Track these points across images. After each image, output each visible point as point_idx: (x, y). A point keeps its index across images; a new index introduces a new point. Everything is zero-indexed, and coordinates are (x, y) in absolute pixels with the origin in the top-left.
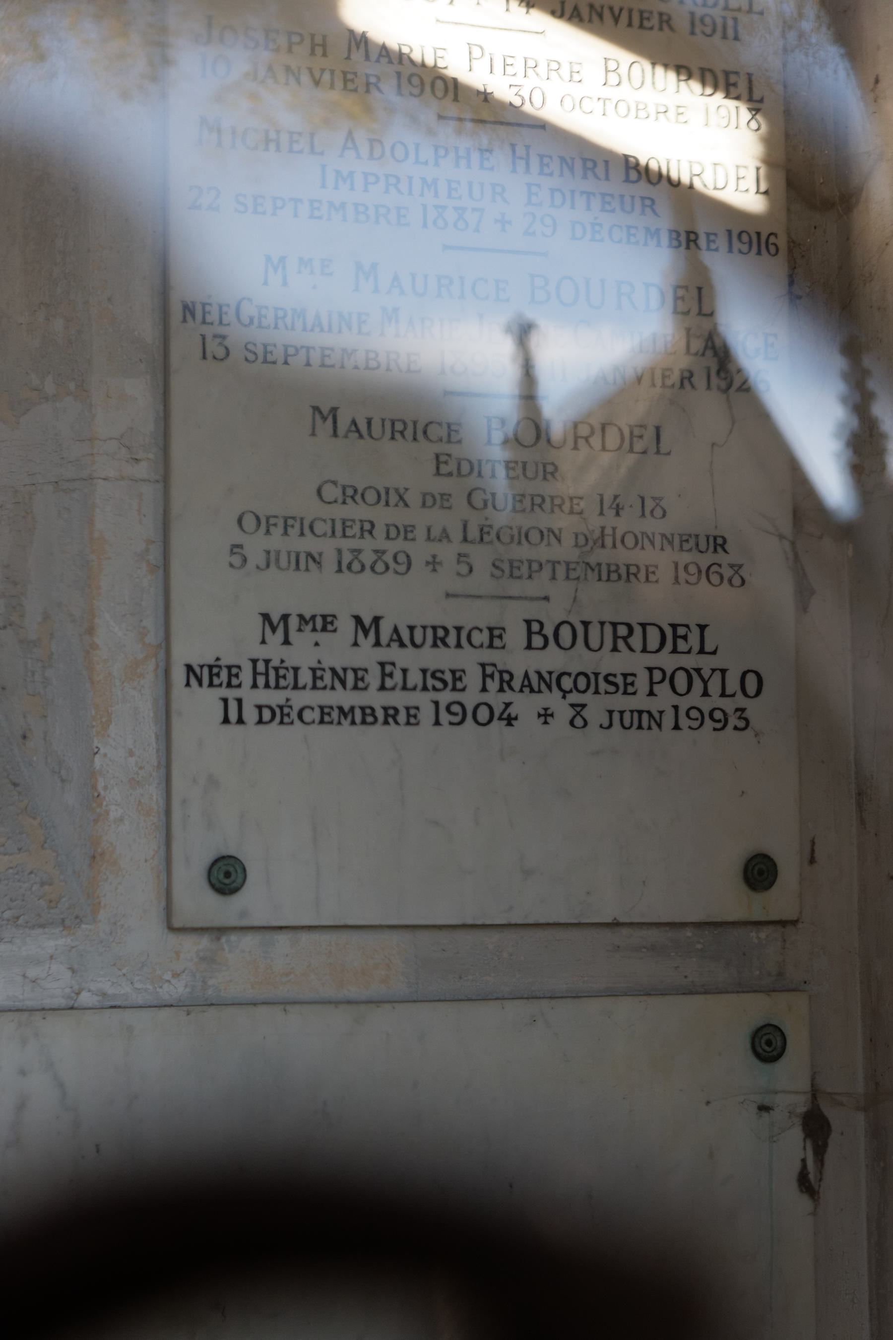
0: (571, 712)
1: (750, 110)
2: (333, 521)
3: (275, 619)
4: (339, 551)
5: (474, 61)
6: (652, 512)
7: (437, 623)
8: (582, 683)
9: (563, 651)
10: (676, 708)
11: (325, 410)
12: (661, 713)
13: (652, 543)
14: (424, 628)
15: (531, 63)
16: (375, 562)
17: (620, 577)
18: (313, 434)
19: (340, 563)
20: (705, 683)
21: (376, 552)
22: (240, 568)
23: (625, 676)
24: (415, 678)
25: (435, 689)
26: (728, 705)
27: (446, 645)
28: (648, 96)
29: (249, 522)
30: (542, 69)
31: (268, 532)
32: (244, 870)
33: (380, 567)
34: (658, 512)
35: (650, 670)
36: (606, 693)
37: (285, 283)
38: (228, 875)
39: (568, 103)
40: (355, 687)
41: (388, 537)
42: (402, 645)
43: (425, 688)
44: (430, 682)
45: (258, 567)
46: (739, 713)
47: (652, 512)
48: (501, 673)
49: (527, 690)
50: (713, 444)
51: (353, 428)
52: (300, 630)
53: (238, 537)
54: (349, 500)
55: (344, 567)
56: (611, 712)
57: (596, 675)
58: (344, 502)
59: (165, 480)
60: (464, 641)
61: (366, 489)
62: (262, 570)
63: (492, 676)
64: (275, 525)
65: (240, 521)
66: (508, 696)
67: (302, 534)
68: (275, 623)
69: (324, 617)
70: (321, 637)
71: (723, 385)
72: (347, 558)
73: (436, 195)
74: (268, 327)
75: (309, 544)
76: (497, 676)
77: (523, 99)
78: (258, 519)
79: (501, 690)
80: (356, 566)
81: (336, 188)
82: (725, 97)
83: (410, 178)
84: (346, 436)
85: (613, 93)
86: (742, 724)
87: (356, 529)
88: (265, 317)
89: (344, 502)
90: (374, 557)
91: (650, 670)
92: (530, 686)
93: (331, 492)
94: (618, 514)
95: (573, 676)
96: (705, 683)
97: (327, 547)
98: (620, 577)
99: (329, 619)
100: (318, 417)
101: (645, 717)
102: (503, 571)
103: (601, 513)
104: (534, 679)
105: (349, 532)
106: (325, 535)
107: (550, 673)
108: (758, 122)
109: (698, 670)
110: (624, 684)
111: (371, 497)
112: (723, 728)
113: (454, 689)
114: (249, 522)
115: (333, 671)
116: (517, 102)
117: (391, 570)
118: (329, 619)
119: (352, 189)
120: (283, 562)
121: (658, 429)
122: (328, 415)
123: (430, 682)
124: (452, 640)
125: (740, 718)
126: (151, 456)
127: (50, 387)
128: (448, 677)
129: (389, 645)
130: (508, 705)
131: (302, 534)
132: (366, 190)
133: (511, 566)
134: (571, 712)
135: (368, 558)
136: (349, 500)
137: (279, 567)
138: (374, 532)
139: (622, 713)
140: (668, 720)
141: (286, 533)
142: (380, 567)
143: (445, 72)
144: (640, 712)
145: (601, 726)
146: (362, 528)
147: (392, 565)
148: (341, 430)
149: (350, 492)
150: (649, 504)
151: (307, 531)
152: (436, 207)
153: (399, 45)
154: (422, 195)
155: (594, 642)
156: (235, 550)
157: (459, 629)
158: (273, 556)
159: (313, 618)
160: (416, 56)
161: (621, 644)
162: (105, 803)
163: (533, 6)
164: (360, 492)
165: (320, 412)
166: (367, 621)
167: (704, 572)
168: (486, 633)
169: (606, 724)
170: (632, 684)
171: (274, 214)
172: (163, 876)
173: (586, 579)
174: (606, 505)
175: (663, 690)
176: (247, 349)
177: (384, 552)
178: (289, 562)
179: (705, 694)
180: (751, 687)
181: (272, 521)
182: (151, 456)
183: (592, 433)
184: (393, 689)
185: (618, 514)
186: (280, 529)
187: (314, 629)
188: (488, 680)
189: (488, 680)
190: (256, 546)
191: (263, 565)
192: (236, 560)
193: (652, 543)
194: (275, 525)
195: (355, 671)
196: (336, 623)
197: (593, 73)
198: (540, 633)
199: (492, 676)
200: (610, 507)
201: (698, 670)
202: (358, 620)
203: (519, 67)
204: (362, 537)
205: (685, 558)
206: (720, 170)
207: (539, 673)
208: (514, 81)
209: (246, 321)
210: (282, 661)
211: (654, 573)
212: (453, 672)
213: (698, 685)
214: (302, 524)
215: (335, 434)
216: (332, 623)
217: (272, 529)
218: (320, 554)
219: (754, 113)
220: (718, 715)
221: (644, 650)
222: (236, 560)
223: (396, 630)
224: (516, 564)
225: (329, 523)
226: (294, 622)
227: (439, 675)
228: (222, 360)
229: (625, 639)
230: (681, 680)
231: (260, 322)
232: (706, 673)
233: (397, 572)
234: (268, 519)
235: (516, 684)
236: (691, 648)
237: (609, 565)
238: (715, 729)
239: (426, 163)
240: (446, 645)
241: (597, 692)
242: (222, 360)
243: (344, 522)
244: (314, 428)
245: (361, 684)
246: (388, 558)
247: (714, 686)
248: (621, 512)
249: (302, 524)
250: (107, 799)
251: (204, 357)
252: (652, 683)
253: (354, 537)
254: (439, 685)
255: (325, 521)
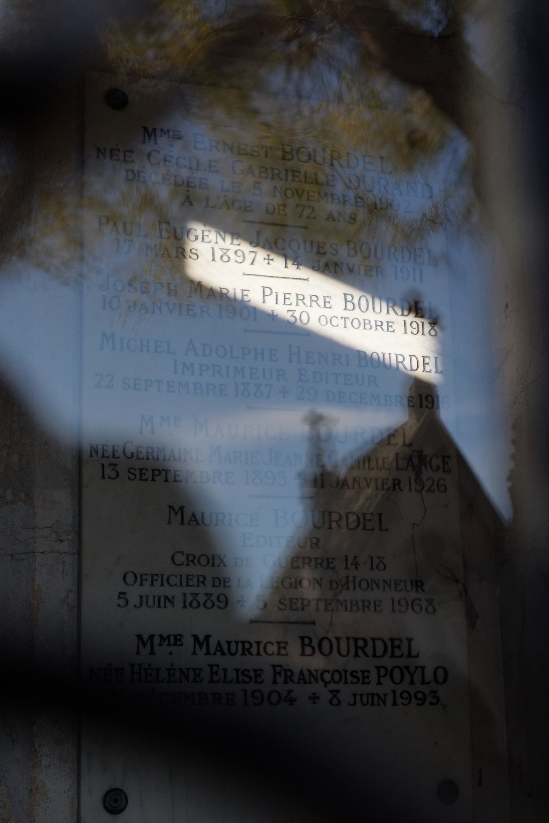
0: (330, 696)
1: (430, 324)
2: (181, 576)
3: (145, 638)
4: (185, 595)
5: (266, 297)
6: (377, 566)
7: (245, 639)
8: (337, 677)
9: (322, 656)
10: (394, 692)
11: (176, 508)
12: (385, 695)
13: (378, 586)
14: (237, 642)
15: (300, 297)
16: (206, 601)
17: (358, 609)
18: (169, 523)
19: (185, 602)
20: (412, 675)
21: (207, 595)
22: (124, 607)
23: (363, 672)
24: (231, 675)
25: (244, 682)
26: (426, 689)
27: (251, 654)
28: (370, 316)
29: (130, 578)
30: (307, 301)
31: (141, 584)
32: (126, 797)
33: (209, 604)
34: (381, 566)
35: (378, 668)
36: (352, 683)
37: (152, 652)
38: (116, 801)
39: (323, 321)
40: (195, 681)
41: (214, 586)
42: (223, 654)
43: (238, 681)
44: (241, 677)
45: (135, 606)
46: (432, 694)
47: (377, 566)
48: (286, 671)
49: (302, 682)
50: (414, 524)
51: (193, 519)
52: (160, 645)
53: (123, 588)
54: (190, 563)
55: (187, 605)
56: (355, 695)
57: (345, 671)
58: (188, 565)
59: (79, 552)
60: (262, 651)
61: (200, 556)
62: (138, 608)
63: (279, 673)
64: (146, 580)
65: (124, 578)
66: (290, 686)
67: (162, 585)
68: (145, 641)
69: (175, 636)
70: (174, 649)
71: (419, 488)
72: (189, 598)
73: (243, 377)
74: (142, 459)
75: (167, 591)
76: (283, 673)
77: (295, 318)
78: (135, 576)
79: (286, 682)
80: (195, 604)
81: (183, 373)
82: (415, 317)
83: (228, 367)
84: (189, 524)
85: (350, 315)
86: (434, 701)
87: (195, 580)
88: (141, 452)
89: (188, 565)
90: (206, 598)
91: (378, 668)
92: (304, 679)
93: (179, 559)
94: (356, 568)
95: (331, 672)
96: (412, 675)
97: (177, 592)
98: (358, 609)
99: (178, 638)
100: (172, 512)
101: (376, 698)
102: (286, 606)
103: (347, 568)
104: (306, 674)
105: (191, 583)
106: (176, 585)
107: (316, 671)
108: (435, 331)
109: (407, 668)
110: (363, 677)
111: (204, 561)
112: (423, 704)
113: (256, 682)
114: (130, 578)
115: (181, 670)
116: (292, 320)
117: (216, 606)
118: (178, 638)
119: (193, 373)
120: (151, 602)
121: (380, 515)
122: (179, 511)
123: (241, 677)
124: (254, 650)
125: (433, 697)
126: (70, 538)
127: (9, 495)
128: (252, 674)
129: (215, 654)
130: (290, 692)
131: (162, 585)
132: (201, 374)
133: (291, 602)
134: (330, 696)
135: (202, 598)
136: (190, 563)
137: (148, 606)
138: (206, 582)
139: (361, 695)
140: (389, 700)
141: (152, 584)
142: (209, 604)
143: (248, 303)
144: (373, 695)
145: (349, 704)
146: (198, 580)
147: (216, 603)
148: (186, 520)
149: (191, 558)
150: (376, 561)
151: (165, 583)
152: (243, 384)
153: (221, 288)
154: (235, 377)
155: (344, 650)
156: (121, 596)
157: (258, 643)
158: (144, 599)
159: (169, 637)
160: (231, 294)
161: (360, 652)
162: (39, 755)
163: (301, 265)
164: (197, 557)
165: (174, 510)
166: (201, 638)
167: (410, 605)
168: (276, 645)
169: (352, 702)
170: (368, 677)
171: (146, 390)
172: (75, 802)
173: (337, 610)
174: (350, 561)
175: (386, 680)
176: (129, 472)
177: (211, 595)
178: (154, 602)
179: (412, 682)
180: (441, 678)
181: (144, 577)
182: (70, 538)
183: (341, 518)
184: (218, 681)
185: (356, 568)
186: (149, 582)
187: (169, 644)
188: (278, 676)
189: (278, 676)
190: (134, 593)
191: (138, 604)
192: (122, 602)
193: (378, 586)
194: (146, 580)
195: (194, 670)
196: (183, 640)
197: (338, 302)
198: (309, 645)
199: (279, 673)
200: (352, 564)
201: (407, 668)
202: (196, 637)
203: (293, 299)
204: (198, 586)
205: (397, 596)
206: (414, 359)
207: (309, 671)
208: (290, 308)
209: (129, 455)
210: (149, 665)
211: (379, 605)
212: (255, 671)
213: (407, 677)
214: (162, 578)
215: (182, 523)
216: (180, 640)
217: (144, 582)
218: (173, 597)
219: (432, 325)
220: (420, 696)
221: (374, 655)
222: (122, 602)
223: (219, 644)
224: (294, 601)
225: (179, 577)
226: (157, 640)
227: (246, 673)
228: (114, 479)
229: (362, 649)
230: (397, 674)
231: (138, 455)
232: (412, 669)
233: (219, 607)
234: (141, 576)
235: (295, 678)
236: (403, 654)
237: (351, 601)
238: (418, 705)
239: (237, 358)
240: (251, 654)
241: (346, 682)
242: (114, 479)
243: (187, 576)
244: (170, 519)
245: (198, 679)
246: (214, 598)
247: (417, 678)
248: (359, 567)
249: (162, 578)
250: (40, 753)
251: (103, 477)
252: (379, 677)
253: (193, 586)
254: (247, 679)
255: (176, 576)
